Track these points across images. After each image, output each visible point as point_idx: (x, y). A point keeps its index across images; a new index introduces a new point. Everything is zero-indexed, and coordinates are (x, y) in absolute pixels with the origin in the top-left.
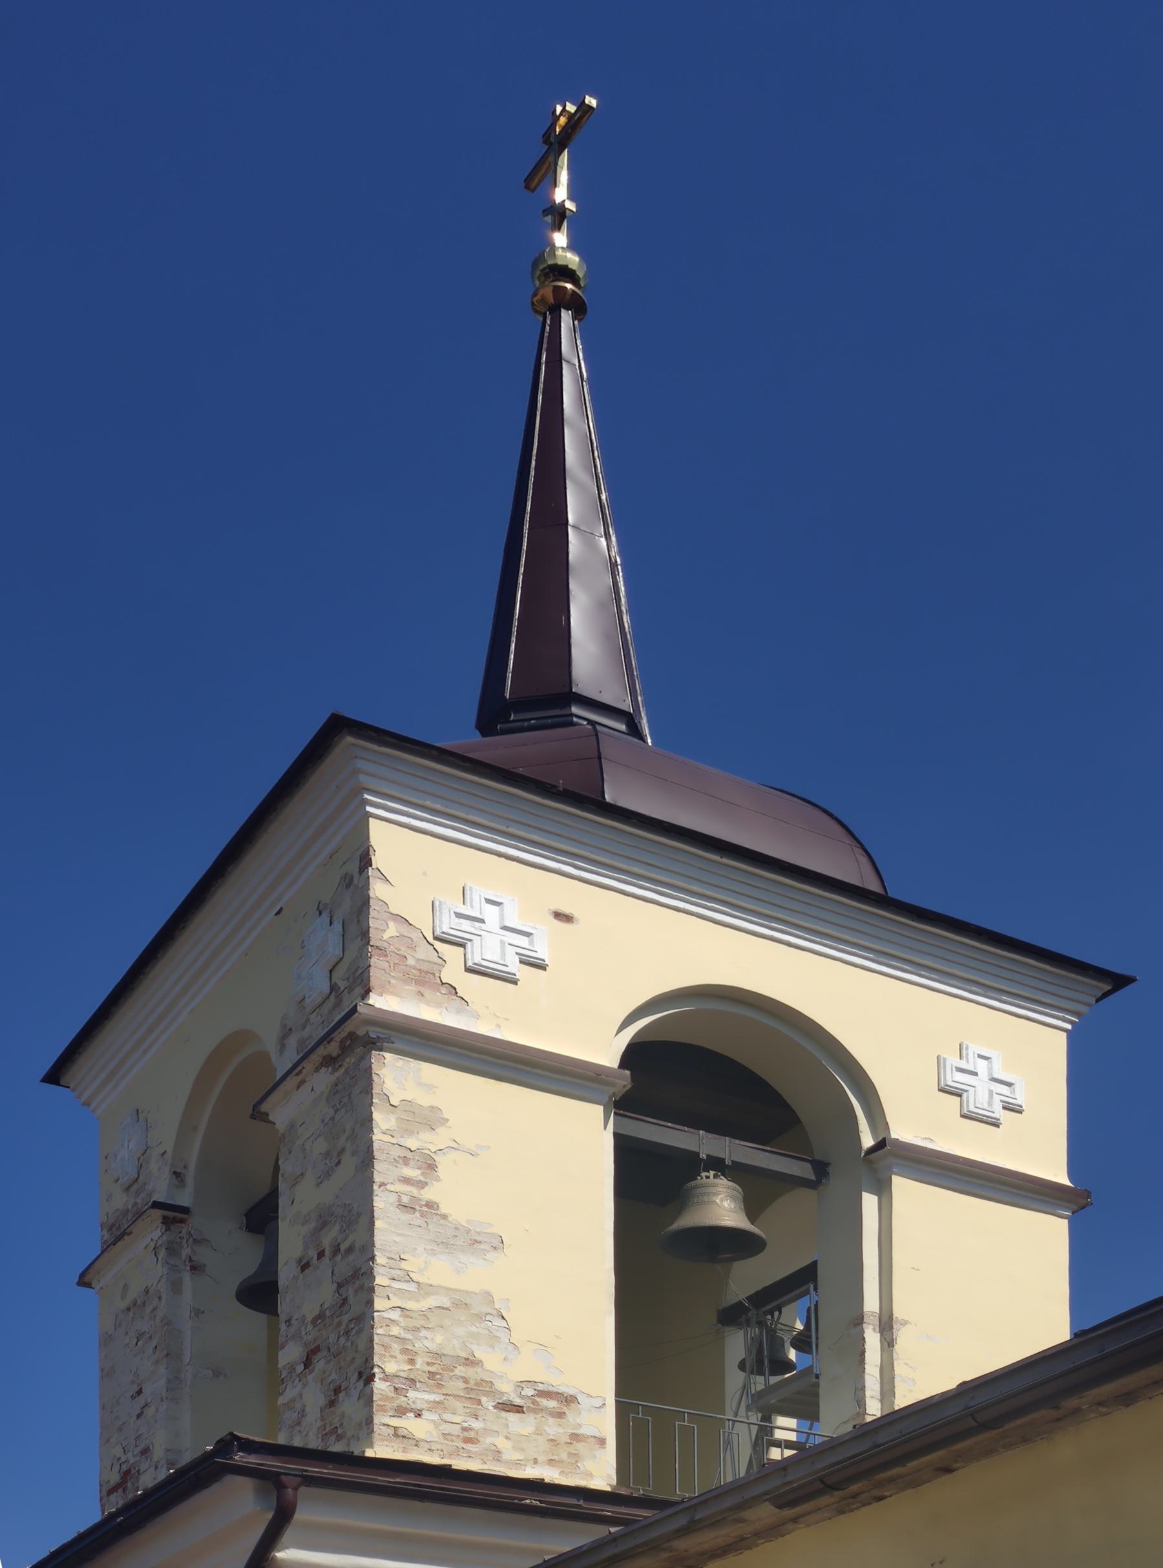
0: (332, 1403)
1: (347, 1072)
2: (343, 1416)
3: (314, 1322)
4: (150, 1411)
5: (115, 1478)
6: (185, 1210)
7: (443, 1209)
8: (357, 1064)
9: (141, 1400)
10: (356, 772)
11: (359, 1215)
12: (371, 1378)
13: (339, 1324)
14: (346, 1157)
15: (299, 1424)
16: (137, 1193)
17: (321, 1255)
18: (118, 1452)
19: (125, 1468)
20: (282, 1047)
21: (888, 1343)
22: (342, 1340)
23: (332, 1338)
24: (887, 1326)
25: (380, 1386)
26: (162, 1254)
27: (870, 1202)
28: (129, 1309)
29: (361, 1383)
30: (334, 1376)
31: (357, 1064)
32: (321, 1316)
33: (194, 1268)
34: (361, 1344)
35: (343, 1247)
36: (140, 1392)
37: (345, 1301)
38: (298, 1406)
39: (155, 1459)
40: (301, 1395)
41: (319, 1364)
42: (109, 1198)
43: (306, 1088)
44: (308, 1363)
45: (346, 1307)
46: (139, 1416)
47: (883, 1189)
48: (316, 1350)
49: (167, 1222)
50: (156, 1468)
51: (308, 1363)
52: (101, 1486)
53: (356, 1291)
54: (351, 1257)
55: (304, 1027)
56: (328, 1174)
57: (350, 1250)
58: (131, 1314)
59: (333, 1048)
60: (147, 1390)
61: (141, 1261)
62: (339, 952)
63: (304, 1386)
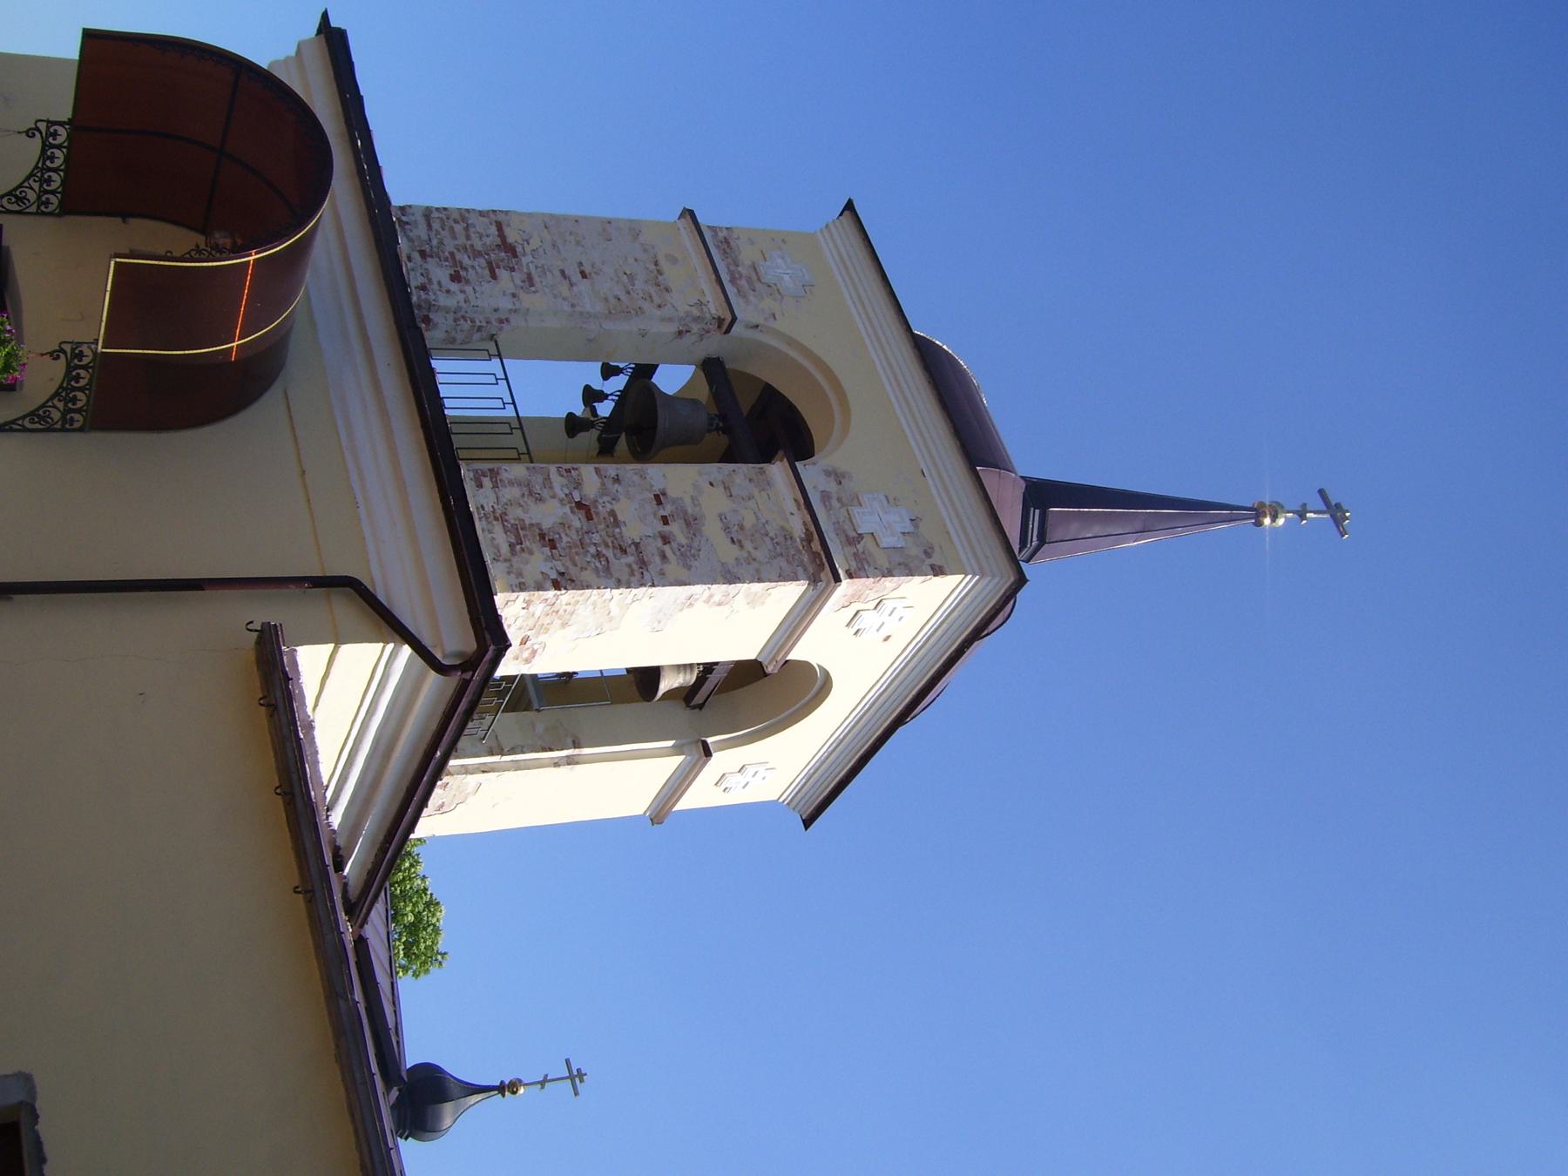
0: (542, 536)
1: (799, 551)
2: (531, 553)
3: (613, 513)
4: (564, 289)
5: (512, 236)
6: (728, 331)
7: (686, 611)
8: (801, 563)
9: (576, 277)
10: (994, 576)
11: (689, 568)
12: (557, 586)
13: (607, 546)
14: (734, 551)
15: (531, 493)
16: (749, 280)
17: (665, 520)
18: (535, 243)
19: (519, 249)
20: (828, 473)
21: (556, 764)
22: (592, 550)
23: (596, 538)
24: (570, 761)
25: (551, 594)
26: (696, 312)
27: (670, 743)
28: (656, 264)
29: (554, 575)
30: (565, 539)
31: (801, 563)
32: (617, 524)
33: (680, 333)
34: (587, 575)
35: (667, 548)
36: (584, 275)
37: (624, 551)
38: (546, 493)
39: (522, 295)
40: (553, 497)
41: (577, 521)
42: (752, 242)
43: (794, 509)
44: (580, 505)
45: (618, 552)
46: (563, 272)
47: (676, 750)
48: (589, 517)
49: (720, 321)
50: (514, 295)
51: (580, 505)
52: (507, 212)
53: (629, 566)
54: (657, 559)
55: (839, 500)
56: (727, 529)
57: (664, 557)
58: (652, 267)
59: (816, 545)
60: (583, 286)
61: (691, 288)
62: (883, 545)
63: (561, 500)
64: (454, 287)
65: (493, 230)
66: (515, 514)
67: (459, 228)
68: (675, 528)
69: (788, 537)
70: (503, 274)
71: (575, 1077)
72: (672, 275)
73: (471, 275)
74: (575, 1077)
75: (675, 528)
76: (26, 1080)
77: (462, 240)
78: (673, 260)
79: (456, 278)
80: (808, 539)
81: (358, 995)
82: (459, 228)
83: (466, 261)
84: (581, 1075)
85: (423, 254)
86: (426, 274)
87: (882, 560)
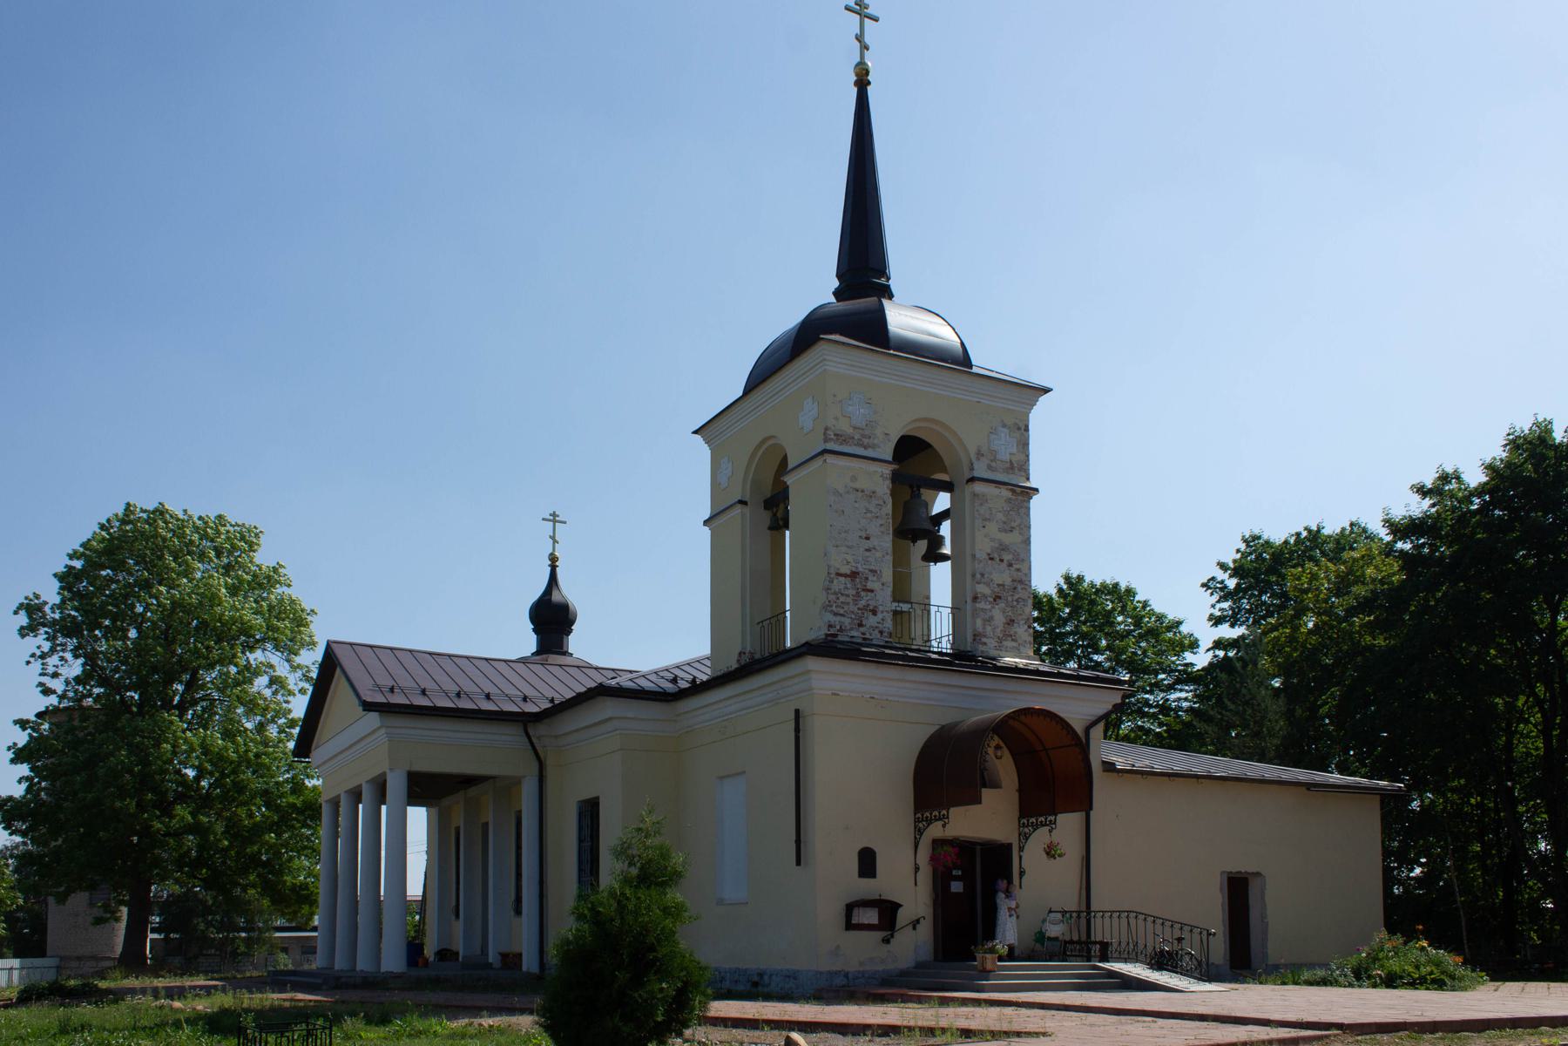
14: (1016, 533)
64: (880, 616)
65: (842, 579)
66: (999, 632)
67: (842, 599)
68: (1007, 557)
69: (1009, 501)
70: (870, 585)
71: (554, 518)
72: (863, 483)
73: (872, 603)
74: (554, 518)
75: (1007, 557)
76: (1223, 873)
77: (849, 600)
78: (854, 479)
79: (874, 612)
80: (1013, 491)
81: (1335, 778)
82: (842, 599)
83: (863, 603)
84: (554, 515)
85: (861, 625)
86: (874, 628)
87: (1023, 457)
